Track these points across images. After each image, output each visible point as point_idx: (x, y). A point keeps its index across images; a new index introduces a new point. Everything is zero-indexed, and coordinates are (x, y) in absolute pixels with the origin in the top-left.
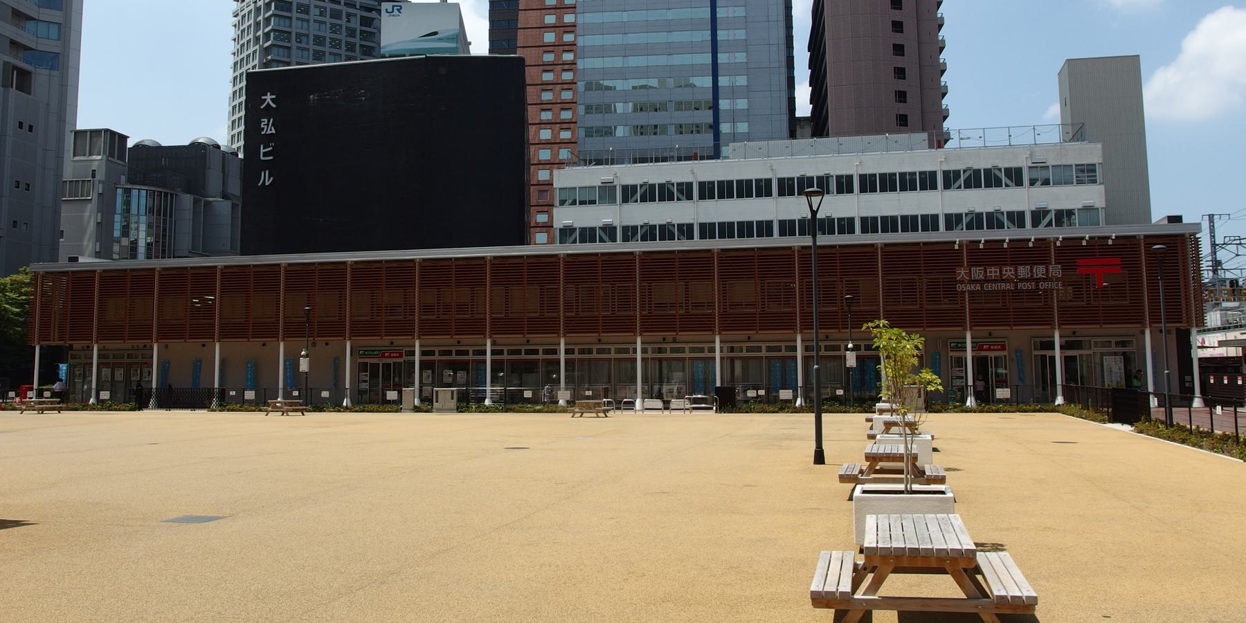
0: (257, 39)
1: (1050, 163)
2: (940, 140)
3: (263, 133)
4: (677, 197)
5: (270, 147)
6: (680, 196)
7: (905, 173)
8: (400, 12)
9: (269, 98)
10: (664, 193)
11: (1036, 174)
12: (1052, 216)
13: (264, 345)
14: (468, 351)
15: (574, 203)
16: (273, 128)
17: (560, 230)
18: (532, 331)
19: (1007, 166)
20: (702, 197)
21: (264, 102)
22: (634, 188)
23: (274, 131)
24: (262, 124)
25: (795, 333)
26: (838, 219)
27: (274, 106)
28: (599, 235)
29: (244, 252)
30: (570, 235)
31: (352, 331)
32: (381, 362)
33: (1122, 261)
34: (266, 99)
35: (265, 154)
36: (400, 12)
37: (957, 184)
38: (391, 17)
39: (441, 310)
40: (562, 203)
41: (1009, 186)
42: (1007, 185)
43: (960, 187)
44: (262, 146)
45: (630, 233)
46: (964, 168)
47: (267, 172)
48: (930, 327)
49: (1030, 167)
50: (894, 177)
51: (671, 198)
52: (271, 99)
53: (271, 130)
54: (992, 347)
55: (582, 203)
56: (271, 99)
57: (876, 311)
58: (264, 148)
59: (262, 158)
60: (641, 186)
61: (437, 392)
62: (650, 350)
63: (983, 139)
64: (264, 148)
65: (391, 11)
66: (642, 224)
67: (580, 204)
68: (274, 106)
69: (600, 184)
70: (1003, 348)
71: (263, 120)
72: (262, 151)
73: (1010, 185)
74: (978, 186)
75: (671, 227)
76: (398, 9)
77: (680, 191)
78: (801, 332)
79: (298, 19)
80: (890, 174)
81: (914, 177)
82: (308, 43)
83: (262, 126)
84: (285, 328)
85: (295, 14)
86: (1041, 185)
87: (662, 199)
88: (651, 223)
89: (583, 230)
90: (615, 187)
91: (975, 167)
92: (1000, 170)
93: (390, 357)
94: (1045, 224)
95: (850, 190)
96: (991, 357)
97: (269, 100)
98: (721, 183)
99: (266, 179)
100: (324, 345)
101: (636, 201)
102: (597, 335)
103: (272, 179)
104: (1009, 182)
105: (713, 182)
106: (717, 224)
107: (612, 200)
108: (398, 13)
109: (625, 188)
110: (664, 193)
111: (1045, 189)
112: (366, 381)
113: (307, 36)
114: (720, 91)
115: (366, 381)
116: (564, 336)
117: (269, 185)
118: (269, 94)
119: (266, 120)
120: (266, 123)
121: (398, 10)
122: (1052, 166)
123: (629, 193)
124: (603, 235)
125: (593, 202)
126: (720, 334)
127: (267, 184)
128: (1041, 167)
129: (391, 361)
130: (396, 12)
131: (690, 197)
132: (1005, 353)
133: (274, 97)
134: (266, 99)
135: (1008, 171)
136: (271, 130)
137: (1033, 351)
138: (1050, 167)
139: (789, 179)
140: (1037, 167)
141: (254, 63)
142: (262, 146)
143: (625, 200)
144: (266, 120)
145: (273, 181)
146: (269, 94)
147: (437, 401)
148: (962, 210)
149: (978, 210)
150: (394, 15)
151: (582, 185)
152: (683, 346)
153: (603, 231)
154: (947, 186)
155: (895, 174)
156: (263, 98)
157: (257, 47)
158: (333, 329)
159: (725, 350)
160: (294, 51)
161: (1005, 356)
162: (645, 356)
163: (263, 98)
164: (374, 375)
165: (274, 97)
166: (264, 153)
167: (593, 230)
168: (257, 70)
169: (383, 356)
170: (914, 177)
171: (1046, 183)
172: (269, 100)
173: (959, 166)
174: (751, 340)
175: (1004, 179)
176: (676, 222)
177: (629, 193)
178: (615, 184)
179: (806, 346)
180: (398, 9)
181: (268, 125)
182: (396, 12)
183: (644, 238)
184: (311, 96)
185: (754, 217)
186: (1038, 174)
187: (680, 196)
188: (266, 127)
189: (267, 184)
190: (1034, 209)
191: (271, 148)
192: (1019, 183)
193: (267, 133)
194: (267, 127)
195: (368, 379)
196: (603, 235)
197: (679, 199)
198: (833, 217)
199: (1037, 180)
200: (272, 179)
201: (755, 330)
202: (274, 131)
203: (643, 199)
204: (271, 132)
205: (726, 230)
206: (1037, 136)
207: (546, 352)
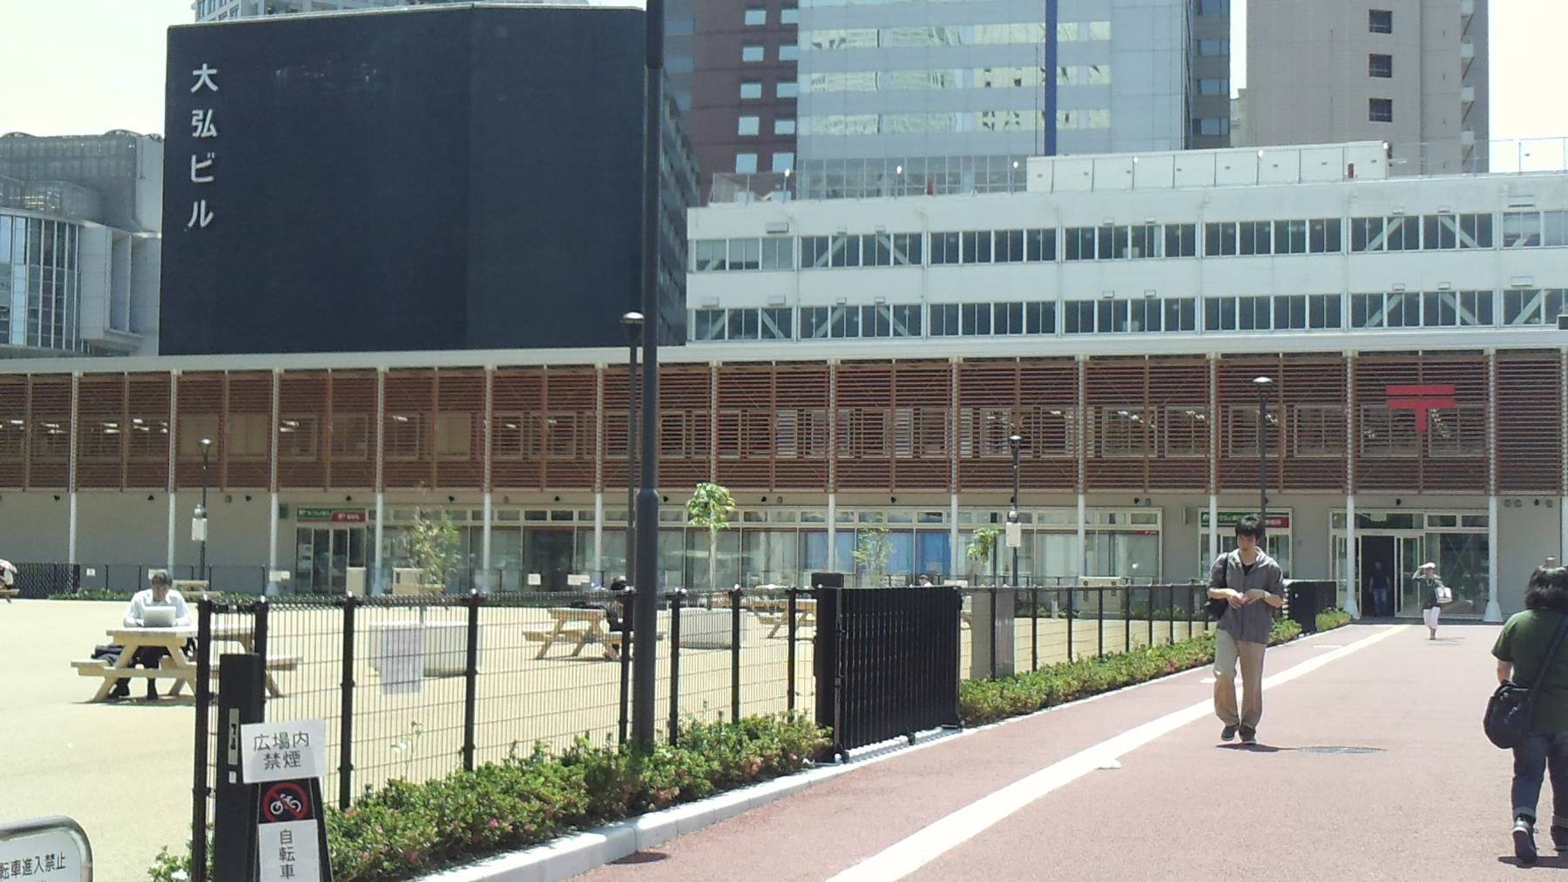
1: (1541, 206)
2: (1475, 159)
3: (196, 135)
4: (895, 259)
5: (207, 159)
7: (1286, 223)
9: (205, 73)
10: (873, 252)
11: (1515, 227)
12: (1541, 300)
13: (151, 498)
14: (571, 513)
15: (721, 266)
16: (212, 127)
17: (698, 312)
18: (1156, 484)
19: (1466, 211)
20: (937, 259)
21: (198, 80)
23: (214, 132)
24: (195, 118)
25: (1208, 493)
26: (1167, 301)
27: (214, 88)
28: (763, 322)
30: (714, 321)
31: (1220, 478)
32: (331, 528)
33: (1457, 389)
34: (199, 76)
35: (200, 173)
37: (1375, 243)
39: (1041, 440)
40: (702, 265)
41: (1467, 247)
42: (1463, 245)
43: (1380, 248)
44: (194, 158)
45: (814, 320)
46: (1390, 214)
47: (203, 203)
48: (967, 486)
49: (1505, 214)
50: (1267, 229)
52: (210, 76)
53: (209, 130)
54: (349, 517)
55: (736, 266)
56: (210, 76)
57: (823, 462)
58: (198, 161)
59: (194, 178)
61: (398, 574)
62: (469, 516)
63: (1523, 154)
64: (198, 161)
68: (214, 88)
69: (767, 236)
70: (1285, 524)
71: (195, 112)
72: (194, 166)
73: (1468, 244)
74: (853, 262)
77: (901, 248)
78: (1217, 493)
80: (1258, 223)
81: (1302, 228)
83: (194, 123)
84: (605, 467)
86: (1525, 245)
87: (869, 262)
89: (736, 315)
90: (790, 240)
91: (851, 232)
92: (1453, 218)
93: (345, 520)
94: (714, 334)
95: (1189, 251)
96: (1399, 540)
97: (205, 78)
99: (201, 214)
100: (1533, 505)
102: (888, 490)
103: (211, 215)
104: (1467, 240)
107: (785, 263)
110: (873, 252)
111: (1532, 252)
112: (309, 558)
115: (309, 558)
116: (958, 492)
117: (207, 226)
118: (205, 66)
119: (201, 113)
120: (201, 117)
122: (1546, 212)
123: (814, 250)
125: (753, 266)
126: (1085, 492)
127: (203, 223)
128: (1525, 214)
129: (347, 527)
131: (915, 259)
132: (1288, 532)
133: (214, 71)
134: (199, 76)
135: (1467, 222)
136: (209, 130)
137: (1331, 528)
138: (1542, 215)
139: (1085, 230)
140: (1518, 213)
142: (194, 158)
143: (808, 263)
144: (201, 113)
145: (213, 219)
146: (205, 66)
147: (1399, 610)
148: (1383, 288)
149: (1410, 289)
152: (1028, 511)
153: (770, 316)
154: (1359, 245)
155: (1234, 225)
156: (196, 73)
158: (250, 475)
159: (496, 517)
161: (1421, 538)
162: (1090, 528)
163: (196, 73)
164: (320, 547)
165: (214, 71)
166: (197, 170)
167: (751, 314)
168: (239, 19)
169: (335, 519)
170: (1302, 228)
171: (1534, 241)
172: (205, 78)
173: (1383, 212)
174: (784, 502)
175: (1457, 229)
177: (814, 250)
178: (790, 234)
179: (607, 513)
181: (204, 121)
183: (1395, 321)
184: (278, 72)
185: (1308, 289)
186: (1522, 227)
187: (901, 258)
188: (200, 124)
189: (203, 223)
190: (1509, 288)
191: (208, 163)
192: (1485, 241)
193: (203, 135)
194: (204, 126)
195: (311, 554)
198: (1158, 297)
199: (1518, 236)
200: (211, 215)
201: (768, 486)
202: (214, 132)
204: (209, 134)
205: (1254, 313)
206: (1176, 173)
207: (1468, 521)
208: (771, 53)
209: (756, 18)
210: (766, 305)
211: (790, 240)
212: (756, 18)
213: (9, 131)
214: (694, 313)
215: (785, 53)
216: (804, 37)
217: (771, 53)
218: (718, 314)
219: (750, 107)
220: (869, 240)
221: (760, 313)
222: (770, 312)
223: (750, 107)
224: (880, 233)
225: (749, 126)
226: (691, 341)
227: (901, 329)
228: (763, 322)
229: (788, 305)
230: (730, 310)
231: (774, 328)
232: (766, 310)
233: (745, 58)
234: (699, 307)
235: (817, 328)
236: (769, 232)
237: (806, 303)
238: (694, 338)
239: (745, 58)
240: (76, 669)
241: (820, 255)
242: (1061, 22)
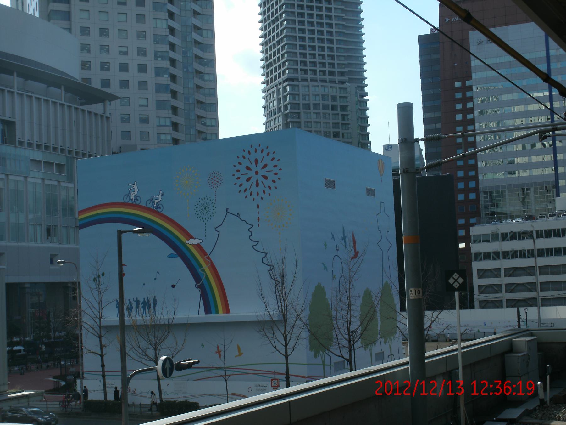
0: (280, 110)
6: (529, 256)
8: (392, 149)
15: (480, 241)
22: (507, 234)
29: (406, 311)
30: (479, 255)
36: (392, 149)
38: (387, 152)
51: (525, 257)
55: (484, 241)
60: (510, 233)
65: (387, 148)
66: (510, 231)
67: (482, 242)
69: (491, 233)
74: (515, 239)
75: (524, 251)
76: (390, 148)
79: (314, 113)
82: (299, 100)
85: (312, 110)
87: (521, 257)
88: (515, 249)
89: (485, 254)
90: (498, 234)
98: (546, 231)
101: (509, 258)
105: (542, 230)
106: (545, 249)
108: (390, 149)
109: (503, 234)
113: (298, 95)
114: (551, 58)
121: (390, 148)
124: (494, 256)
125: (488, 241)
130: (390, 149)
141: (279, 124)
143: (503, 239)
150: (389, 151)
151: (483, 234)
157: (281, 114)
160: (302, 115)
167: (489, 253)
176: (526, 249)
178: (498, 232)
180: (390, 148)
182: (390, 149)
196: (494, 256)
197: (528, 257)
203: (511, 239)
208: (464, 94)
209: (458, 84)
210: (492, 251)
211: (498, 234)
212: (458, 84)
213: (271, 187)
214: (474, 254)
215: (469, 94)
216: (474, 89)
217: (464, 94)
218: (480, 254)
219: (459, 111)
220: (520, 251)
221: (491, 253)
222: (494, 253)
223: (459, 111)
224: (523, 250)
225: (459, 117)
226: (473, 261)
227: (529, 256)
228: (492, 256)
229: (499, 250)
230: (483, 253)
231: (495, 257)
232: (492, 252)
233: (456, 97)
234: (475, 252)
235: (507, 256)
236: (492, 232)
237: (504, 250)
238: (474, 260)
239: (456, 97)
240: (49, 237)
241: (506, 237)
242: (559, 167)
